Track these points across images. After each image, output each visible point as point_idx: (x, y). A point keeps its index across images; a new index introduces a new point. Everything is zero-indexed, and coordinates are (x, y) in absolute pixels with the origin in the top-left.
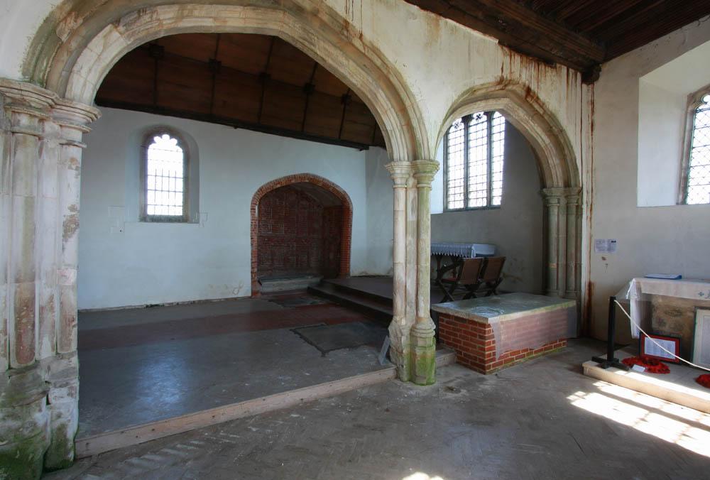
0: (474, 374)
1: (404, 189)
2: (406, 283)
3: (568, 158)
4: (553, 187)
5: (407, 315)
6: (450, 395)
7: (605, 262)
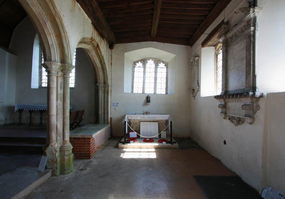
0: (86, 161)
1: (56, 77)
2: (57, 125)
3: (105, 73)
4: (100, 83)
5: (58, 141)
6: (84, 172)
7: (115, 110)
